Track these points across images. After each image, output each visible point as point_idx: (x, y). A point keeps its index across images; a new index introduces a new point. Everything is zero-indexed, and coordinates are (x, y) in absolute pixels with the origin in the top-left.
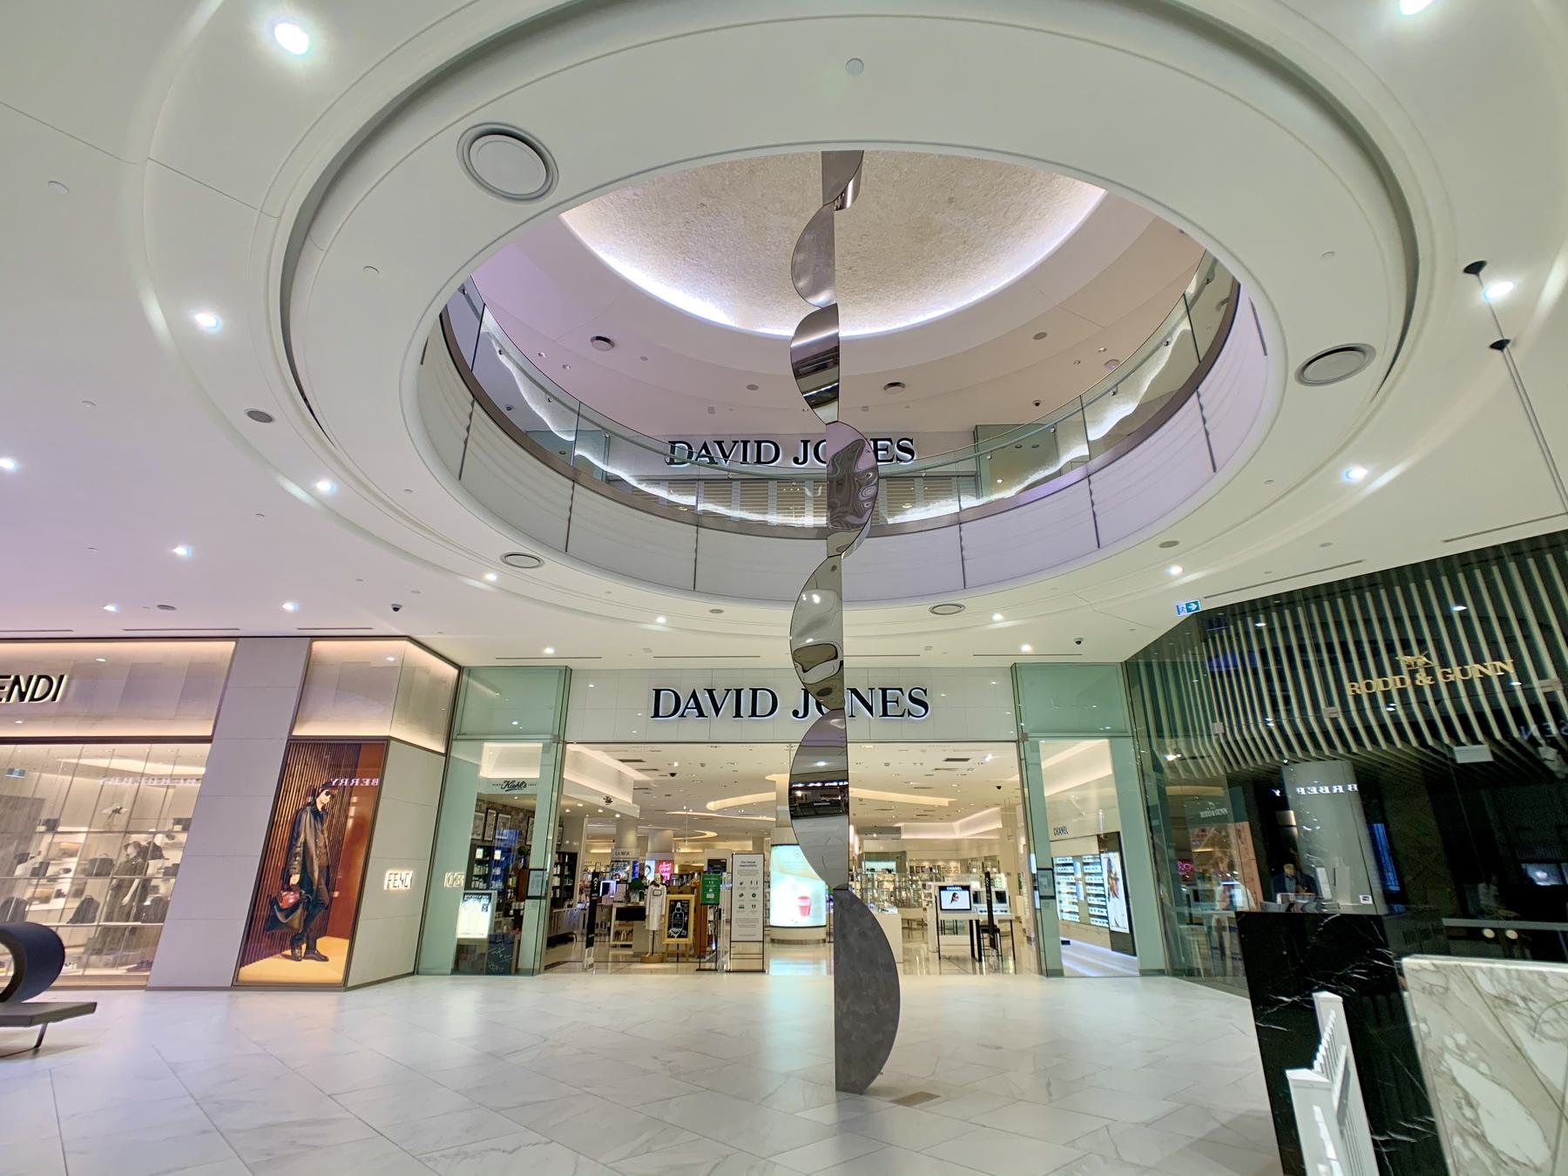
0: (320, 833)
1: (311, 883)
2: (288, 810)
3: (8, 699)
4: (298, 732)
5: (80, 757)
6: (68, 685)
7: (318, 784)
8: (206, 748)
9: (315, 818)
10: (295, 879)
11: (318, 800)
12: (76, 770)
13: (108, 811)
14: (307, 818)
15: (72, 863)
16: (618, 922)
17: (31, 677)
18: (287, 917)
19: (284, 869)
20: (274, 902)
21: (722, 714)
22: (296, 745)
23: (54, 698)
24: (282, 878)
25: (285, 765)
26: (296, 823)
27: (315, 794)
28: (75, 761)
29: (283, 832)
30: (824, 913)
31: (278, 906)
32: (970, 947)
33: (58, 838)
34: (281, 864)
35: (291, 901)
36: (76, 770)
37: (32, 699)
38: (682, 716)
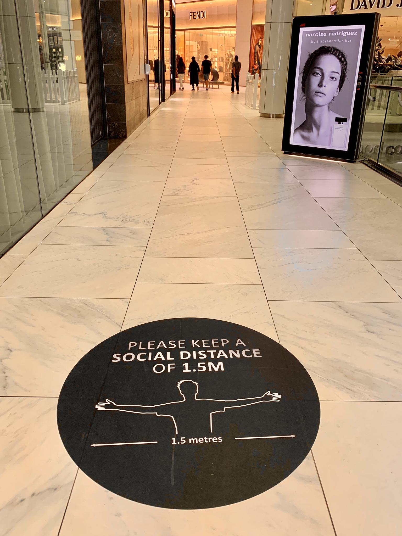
0: (260, 51)
1: (260, 63)
2: (253, 46)
3: (197, 18)
4: (253, 24)
5: (212, 31)
6: (206, 12)
7: (259, 38)
8: (235, 29)
9: (259, 47)
10: (256, 62)
11: (259, 42)
12: (212, 34)
13: (220, 46)
14: (257, 47)
15: (216, 59)
16: (379, 84)
17: (200, 12)
18: (256, 71)
19: (254, 60)
20: (253, 68)
21: (373, 8)
22: (253, 27)
23: (205, 18)
24: (254, 62)
25: (251, 33)
26: (255, 49)
27: (258, 41)
28: (212, 32)
29: (253, 51)
30: (63, 43)
31: (254, 69)
32: (148, 49)
33: (213, 52)
34: (253, 59)
35: (256, 67)
36: (212, 34)
37: (201, 18)
38: (360, 8)
